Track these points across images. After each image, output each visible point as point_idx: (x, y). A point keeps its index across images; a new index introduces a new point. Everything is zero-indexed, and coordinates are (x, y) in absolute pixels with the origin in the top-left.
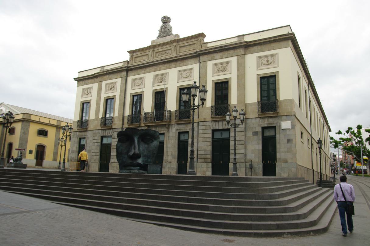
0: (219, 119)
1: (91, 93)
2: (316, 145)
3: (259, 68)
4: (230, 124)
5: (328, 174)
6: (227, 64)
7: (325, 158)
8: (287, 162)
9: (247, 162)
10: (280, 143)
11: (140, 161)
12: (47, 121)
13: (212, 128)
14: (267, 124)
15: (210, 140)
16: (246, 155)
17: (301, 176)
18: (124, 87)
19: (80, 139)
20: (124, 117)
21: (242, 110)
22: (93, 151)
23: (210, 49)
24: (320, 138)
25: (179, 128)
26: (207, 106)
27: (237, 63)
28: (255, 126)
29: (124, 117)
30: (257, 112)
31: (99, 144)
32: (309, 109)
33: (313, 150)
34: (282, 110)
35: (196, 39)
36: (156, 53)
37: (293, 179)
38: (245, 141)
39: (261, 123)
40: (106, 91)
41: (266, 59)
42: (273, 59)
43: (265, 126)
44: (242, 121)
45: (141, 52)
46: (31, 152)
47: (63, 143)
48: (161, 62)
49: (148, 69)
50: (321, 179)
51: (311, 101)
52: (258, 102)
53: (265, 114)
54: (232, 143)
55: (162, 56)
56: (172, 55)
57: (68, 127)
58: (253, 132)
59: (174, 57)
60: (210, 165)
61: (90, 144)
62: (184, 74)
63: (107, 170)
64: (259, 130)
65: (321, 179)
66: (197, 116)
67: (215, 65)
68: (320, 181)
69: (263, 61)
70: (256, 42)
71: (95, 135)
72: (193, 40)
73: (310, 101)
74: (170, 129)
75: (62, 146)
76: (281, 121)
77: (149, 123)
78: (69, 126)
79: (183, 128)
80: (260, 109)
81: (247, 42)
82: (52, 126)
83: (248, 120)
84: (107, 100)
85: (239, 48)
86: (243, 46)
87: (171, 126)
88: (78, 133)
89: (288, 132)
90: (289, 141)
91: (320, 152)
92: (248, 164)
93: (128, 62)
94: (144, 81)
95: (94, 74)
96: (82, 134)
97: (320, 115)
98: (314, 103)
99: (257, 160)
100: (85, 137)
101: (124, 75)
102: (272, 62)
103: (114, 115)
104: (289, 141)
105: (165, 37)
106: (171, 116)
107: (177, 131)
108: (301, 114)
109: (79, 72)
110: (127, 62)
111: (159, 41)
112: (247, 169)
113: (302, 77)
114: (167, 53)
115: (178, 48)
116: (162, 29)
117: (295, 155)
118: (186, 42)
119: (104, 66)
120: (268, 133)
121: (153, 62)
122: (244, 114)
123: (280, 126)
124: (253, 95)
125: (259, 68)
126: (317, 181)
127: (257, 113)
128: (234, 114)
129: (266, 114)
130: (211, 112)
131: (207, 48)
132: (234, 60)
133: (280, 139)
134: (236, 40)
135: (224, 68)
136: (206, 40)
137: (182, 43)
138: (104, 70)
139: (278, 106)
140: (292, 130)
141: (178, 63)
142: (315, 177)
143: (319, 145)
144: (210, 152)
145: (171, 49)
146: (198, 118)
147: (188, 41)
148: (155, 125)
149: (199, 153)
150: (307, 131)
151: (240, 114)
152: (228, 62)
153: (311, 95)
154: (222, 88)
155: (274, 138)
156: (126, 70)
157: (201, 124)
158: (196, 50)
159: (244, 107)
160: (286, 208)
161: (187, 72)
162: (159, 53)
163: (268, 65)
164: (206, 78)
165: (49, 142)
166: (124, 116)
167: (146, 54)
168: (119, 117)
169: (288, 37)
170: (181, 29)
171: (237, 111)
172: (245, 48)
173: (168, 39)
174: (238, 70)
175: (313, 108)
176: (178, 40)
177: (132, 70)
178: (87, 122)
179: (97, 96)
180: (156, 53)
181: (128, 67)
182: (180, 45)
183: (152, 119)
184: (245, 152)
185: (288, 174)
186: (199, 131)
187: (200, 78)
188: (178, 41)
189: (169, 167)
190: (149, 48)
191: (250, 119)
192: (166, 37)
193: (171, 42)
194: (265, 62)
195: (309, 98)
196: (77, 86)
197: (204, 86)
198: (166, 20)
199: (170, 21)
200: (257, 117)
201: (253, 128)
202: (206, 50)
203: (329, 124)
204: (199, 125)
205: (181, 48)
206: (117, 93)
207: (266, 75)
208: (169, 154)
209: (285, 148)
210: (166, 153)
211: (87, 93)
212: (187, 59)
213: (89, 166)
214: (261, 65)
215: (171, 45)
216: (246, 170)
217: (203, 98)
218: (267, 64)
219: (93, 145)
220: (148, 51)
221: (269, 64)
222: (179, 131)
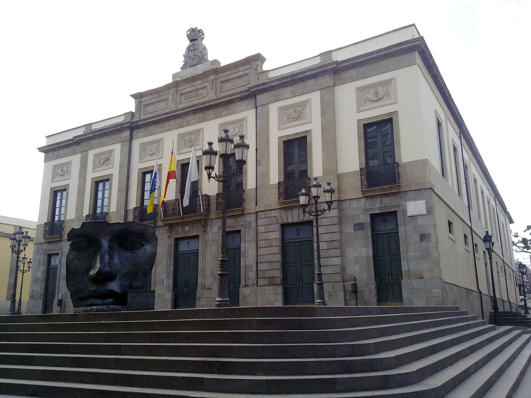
0: (292, 205)
1: (69, 173)
2: (482, 247)
3: (361, 109)
5: (513, 301)
6: (303, 107)
7: (505, 270)
8: (422, 278)
9: (347, 281)
10: (406, 243)
11: (114, 286)
13: (280, 221)
14: (381, 208)
15: (278, 243)
16: (343, 268)
17: (454, 302)
18: (127, 158)
19: (50, 256)
20: (126, 211)
21: (329, 184)
23: (271, 82)
29: (126, 211)
30: (360, 188)
32: (463, 181)
33: (476, 255)
34: (407, 180)
35: (248, 66)
36: (181, 95)
37: (436, 309)
38: (340, 241)
39: (368, 207)
40: (94, 168)
41: (372, 91)
42: (385, 90)
43: (376, 212)
45: (155, 96)
47: (26, 266)
48: (189, 111)
49: (167, 124)
50: (495, 308)
51: (469, 167)
52: (361, 169)
53: (374, 190)
56: (208, 97)
57: (21, 235)
59: (211, 101)
60: (280, 289)
64: (367, 219)
65: (495, 308)
66: (255, 201)
69: (367, 95)
70: (354, 62)
72: (244, 68)
73: (465, 167)
74: (209, 228)
75: (23, 272)
76: (407, 200)
77: (171, 220)
78: (23, 233)
80: (365, 182)
81: (337, 63)
82: (5, 236)
83: (344, 202)
84: (96, 183)
85: (323, 75)
86: (329, 71)
87: (209, 223)
88: (45, 246)
89: (420, 221)
90: (423, 237)
91: (490, 258)
92: (349, 284)
94: (161, 146)
96: (52, 246)
97: (487, 193)
98: (474, 170)
99: (365, 276)
100: (58, 252)
101: (126, 137)
102: (384, 95)
103: (65, 217)
104: (423, 237)
106: (209, 205)
108: (447, 187)
109: (47, 137)
110: (130, 114)
111: (186, 74)
112: (348, 293)
113: (446, 121)
116: (190, 53)
117: (437, 263)
118: (232, 72)
119: (91, 124)
121: (175, 111)
122: (332, 191)
123: (405, 211)
124: (351, 159)
125: (361, 109)
126: (491, 313)
127: (360, 190)
128: (314, 191)
129: (377, 190)
130: (277, 193)
131: (268, 81)
132: (315, 99)
133: (405, 235)
134: (317, 61)
135: (297, 113)
136: (266, 67)
137: (225, 74)
138: (91, 130)
139: (399, 174)
140: (428, 216)
141: (220, 110)
142: (484, 306)
143: (488, 244)
144: (278, 265)
145: (209, 87)
146: (256, 205)
147: (234, 71)
148: (181, 222)
149: (259, 268)
150: (464, 222)
151: (326, 191)
152: (305, 103)
153: (467, 156)
154: (295, 148)
156: (129, 128)
157: (261, 215)
158: (249, 85)
159: (336, 180)
161: (235, 125)
162: (186, 95)
163: (377, 101)
166: (127, 210)
167: (163, 98)
168: (118, 212)
169: (414, 46)
170: (223, 51)
171: (318, 186)
172: (335, 74)
173: (200, 69)
174: (323, 115)
175: (473, 182)
176: (217, 69)
177: (138, 127)
178: (61, 223)
180: (181, 95)
181: (131, 123)
182: (222, 79)
183: (177, 211)
184: (342, 262)
185: (427, 300)
186: (259, 228)
187: (257, 134)
188: (217, 71)
189: (207, 298)
190: (167, 87)
191: (348, 202)
193: (206, 75)
194: (372, 97)
195: (463, 160)
196: (44, 162)
197: (242, 137)
198: (195, 36)
199: (204, 37)
200: (361, 196)
202: (265, 84)
203: (508, 210)
205: (223, 84)
206: (114, 170)
207: (374, 121)
208: (208, 272)
209: (416, 251)
210: (202, 272)
212: (234, 103)
213: (65, 306)
214: (365, 102)
216: (345, 295)
217: (241, 159)
218: (375, 99)
220: (166, 92)
221: (379, 100)
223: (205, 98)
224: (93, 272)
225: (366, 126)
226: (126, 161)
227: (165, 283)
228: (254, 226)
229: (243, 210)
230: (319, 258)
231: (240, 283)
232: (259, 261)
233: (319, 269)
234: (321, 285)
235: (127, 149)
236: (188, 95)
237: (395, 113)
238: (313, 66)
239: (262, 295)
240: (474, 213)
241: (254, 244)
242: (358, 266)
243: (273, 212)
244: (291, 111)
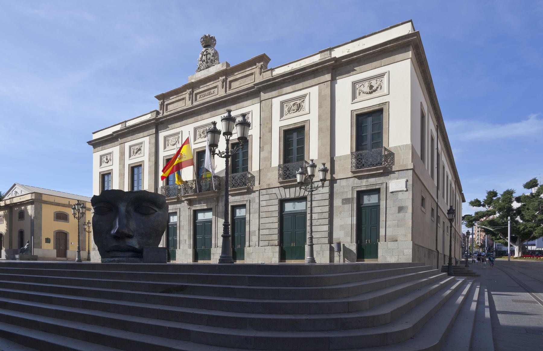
2: (444, 219)
4: (218, 153)
11: (134, 243)
12: (66, 202)
13: (279, 197)
24: (451, 207)
28: (346, 190)
32: (435, 166)
33: (439, 225)
41: (367, 84)
42: (379, 82)
46: (48, 240)
54: (308, 216)
58: (343, 200)
59: (222, 98)
60: (277, 249)
68: (448, 266)
69: (362, 88)
76: (390, 179)
93: (158, 113)
98: (444, 159)
102: (377, 88)
120: (368, 200)
130: (277, 174)
142: (439, 261)
144: (276, 231)
149: (261, 233)
154: (294, 140)
155: (377, 207)
156: (158, 124)
160: (386, 334)
165: (70, 227)
167: (182, 97)
169: (409, 42)
179: (120, 164)
199: (215, 44)
201: (343, 192)
206: (145, 158)
207: (366, 111)
211: (106, 161)
215: (217, 80)
224: (112, 232)
225: (358, 116)
227: (187, 242)
228: (257, 201)
230: (311, 225)
231: (245, 244)
232: (261, 228)
233: (311, 234)
234: (311, 246)
235: (153, 141)
237: (387, 103)
239: (261, 251)
240: (440, 192)
242: (343, 232)
243: (273, 189)
244: (292, 103)
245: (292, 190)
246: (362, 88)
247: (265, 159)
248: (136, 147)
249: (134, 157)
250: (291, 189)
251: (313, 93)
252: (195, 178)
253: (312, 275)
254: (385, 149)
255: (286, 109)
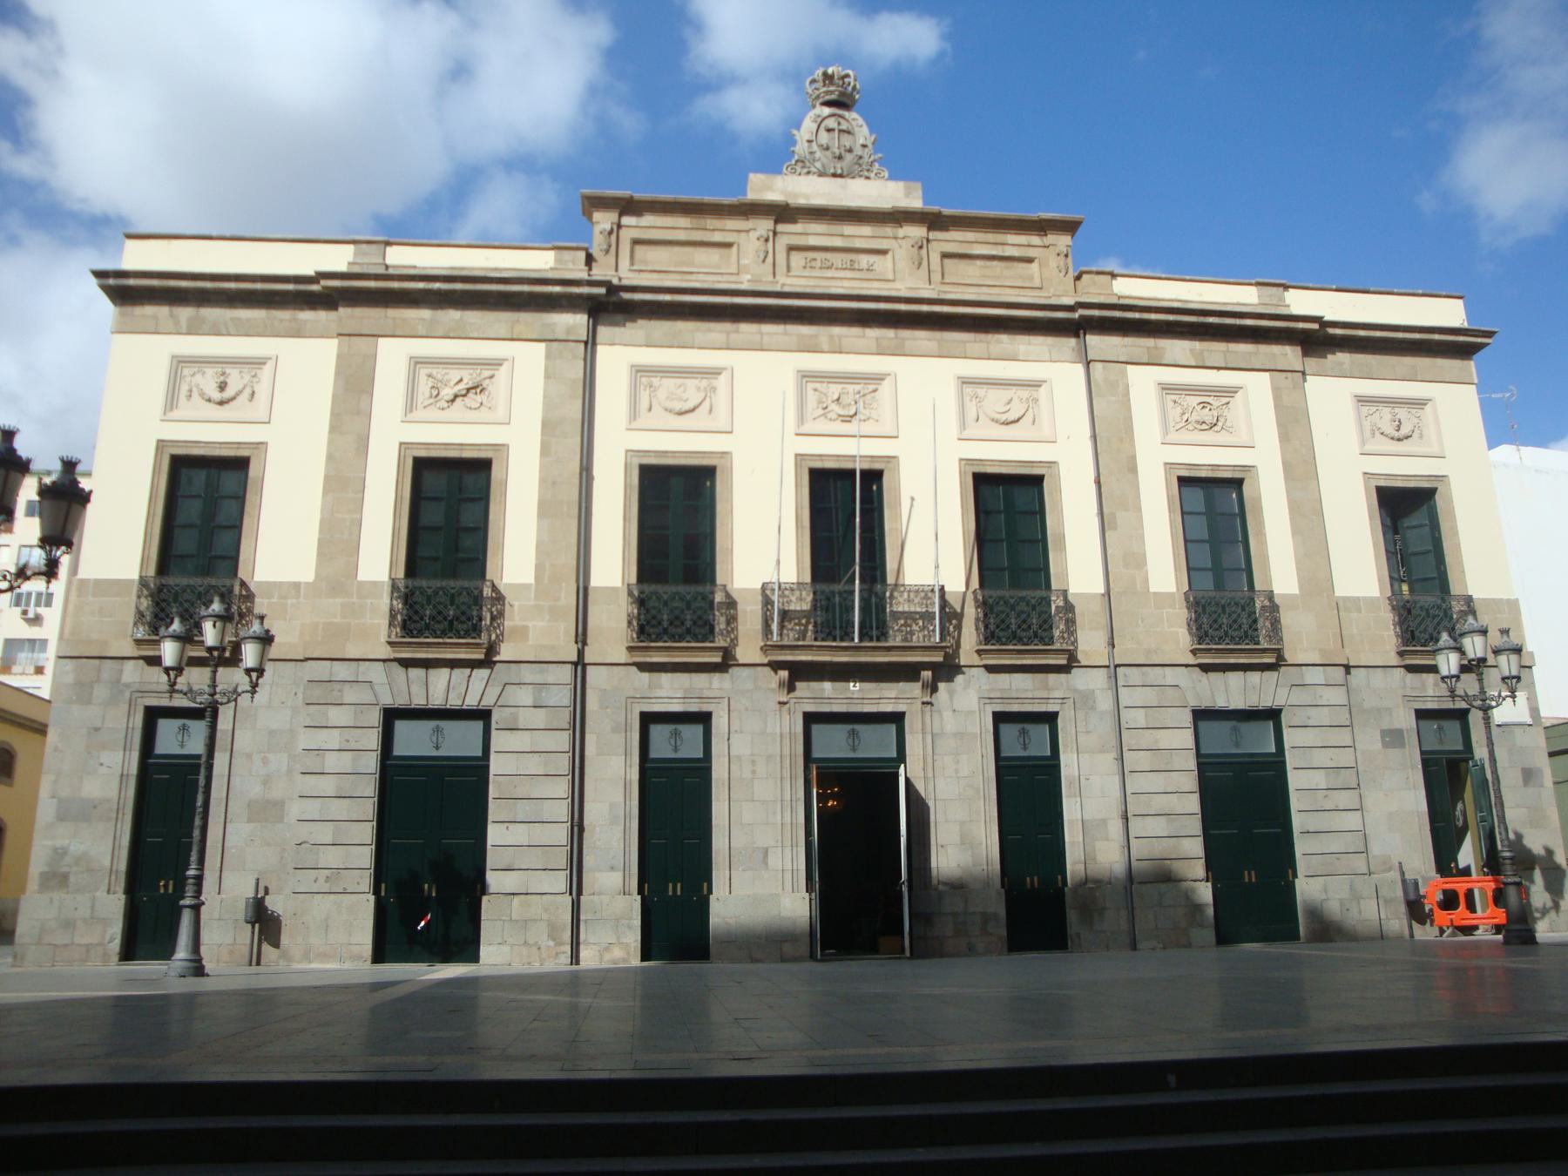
6: (1225, 400)
20: (584, 593)
22: (296, 809)
25: (1001, 690)
26: (360, 578)
27: (1276, 407)
31: (371, 763)
43: (1430, 706)
44: (254, 675)
55: (830, 274)
58: (1384, 733)
61: (265, 762)
62: (994, 400)
63: (460, 940)
67: (417, 362)
71: (322, 695)
79: (1024, 691)
95: (312, 273)
105: (839, 180)
107: (989, 710)
114: (864, 265)
115: (935, 258)
124: (1359, 565)
147: (991, 237)
164: (1133, 446)
167: (717, 237)
180: (792, 249)
187: (1094, 437)
192: (849, 181)
204: (1120, 683)
207: (1203, 474)
211: (217, 396)
219: (312, 763)
222: (999, 708)
223: (889, 285)
225: (1184, 481)
226: (575, 410)
228: (1105, 703)
229: (492, 649)
236: (819, 256)
238: (496, 269)
241: (1108, 761)
245: (440, 677)
246: (198, 379)
247: (338, 539)
248: (455, 375)
249: (433, 413)
250: (457, 672)
251: (304, 359)
252: (807, 578)
253: (1350, 1014)
254: (243, 584)
255: (424, 386)
